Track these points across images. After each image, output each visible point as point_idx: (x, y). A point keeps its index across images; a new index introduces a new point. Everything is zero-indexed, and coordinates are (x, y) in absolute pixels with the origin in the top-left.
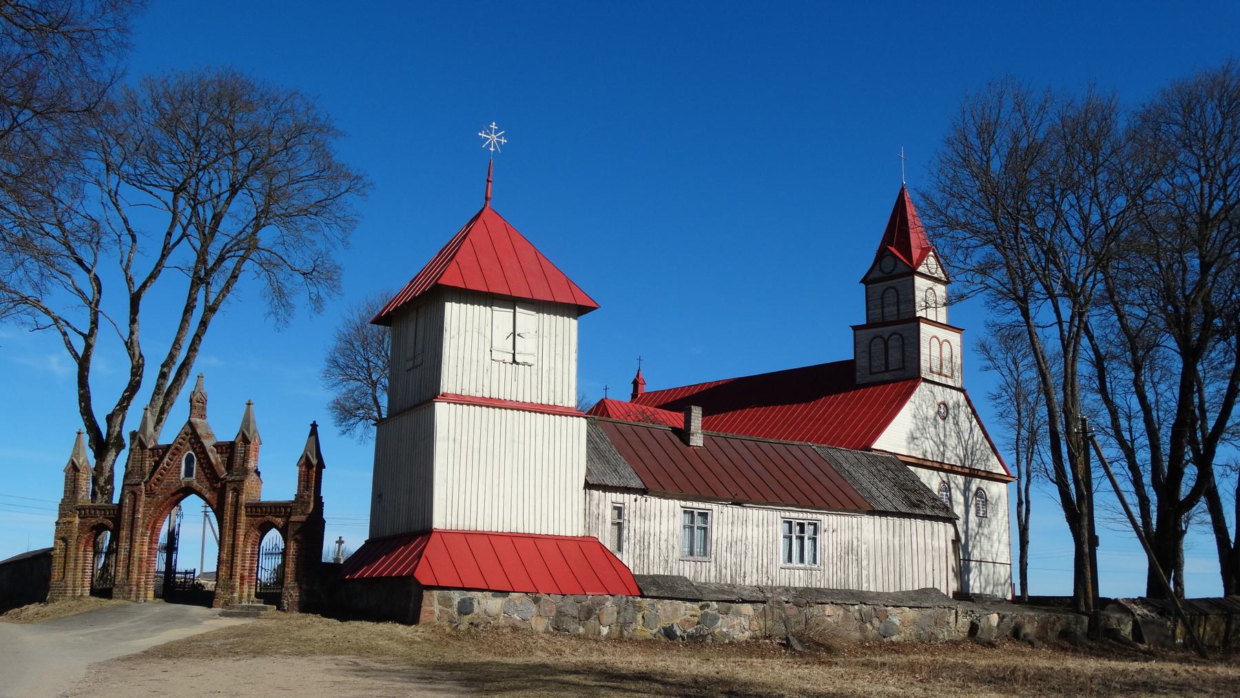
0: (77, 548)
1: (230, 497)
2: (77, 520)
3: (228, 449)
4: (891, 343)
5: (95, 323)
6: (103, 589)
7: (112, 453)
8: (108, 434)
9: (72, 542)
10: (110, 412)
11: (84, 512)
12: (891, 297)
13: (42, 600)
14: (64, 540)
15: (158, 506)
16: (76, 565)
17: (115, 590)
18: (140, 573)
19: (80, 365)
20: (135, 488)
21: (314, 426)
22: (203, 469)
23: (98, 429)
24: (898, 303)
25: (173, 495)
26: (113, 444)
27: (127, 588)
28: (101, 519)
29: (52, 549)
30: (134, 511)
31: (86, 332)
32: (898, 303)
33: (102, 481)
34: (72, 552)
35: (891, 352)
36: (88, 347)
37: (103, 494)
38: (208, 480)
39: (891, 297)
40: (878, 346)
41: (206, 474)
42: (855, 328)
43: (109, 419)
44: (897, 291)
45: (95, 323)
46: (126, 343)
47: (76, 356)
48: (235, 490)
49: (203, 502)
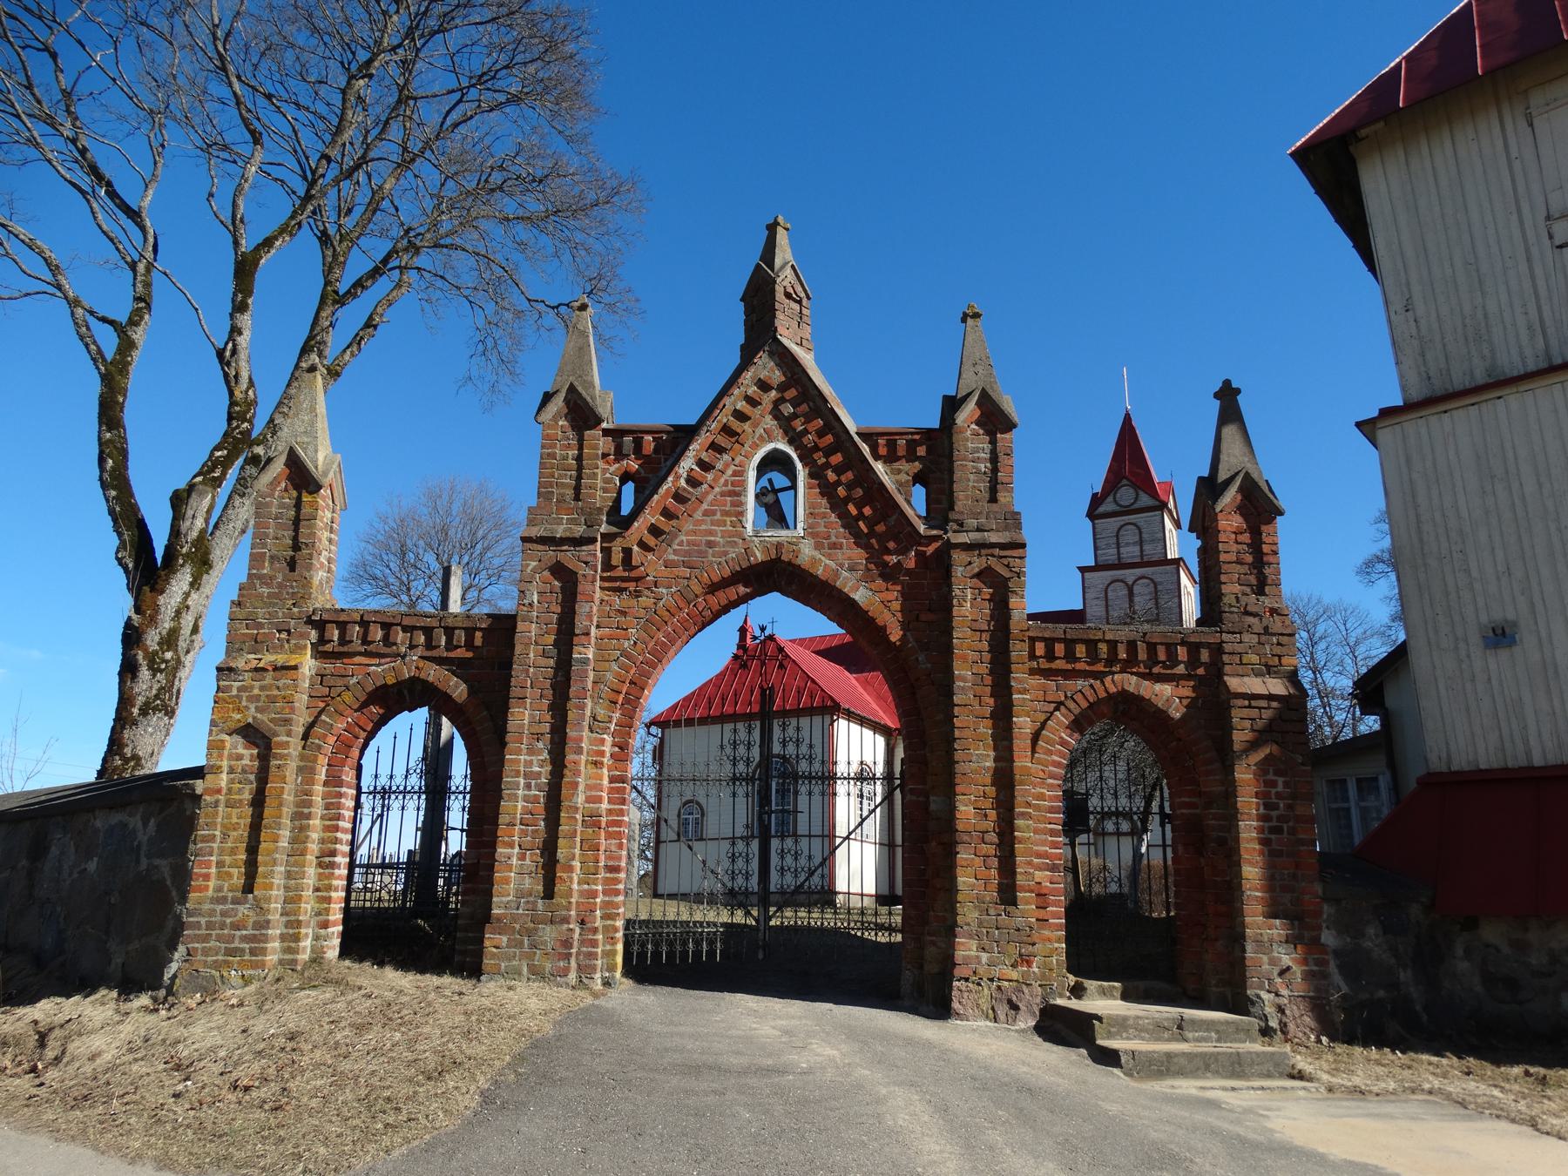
0: (307, 771)
1: (969, 606)
2: (308, 665)
3: (932, 453)
4: (1136, 589)
5: (143, 301)
6: (425, 924)
7: (180, 582)
8: (175, 533)
9: (290, 747)
10: (182, 485)
11: (335, 636)
12: (1130, 535)
13: (138, 976)
14: (250, 733)
15: (652, 623)
16: (300, 837)
17: (494, 941)
18: (589, 873)
19: (107, 379)
20: (568, 557)
21: (1228, 395)
22: (837, 505)
23: (141, 526)
24: (1141, 542)
25: (713, 588)
26: (187, 556)
27: (549, 934)
28: (412, 665)
29: (198, 773)
30: (566, 634)
31: (123, 318)
32: (1141, 542)
33: (152, 639)
34: (286, 786)
35: (1137, 599)
36: (126, 346)
37: (155, 671)
38: (860, 540)
39: (1130, 535)
40: (1120, 592)
41: (849, 523)
42: (1083, 570)
43: (179, 501)
44: (1139, 528)
45: (143, 301)
46: (220, 354)
47: (97, 357)
48: (986, 575)
49: (1382, 505)
